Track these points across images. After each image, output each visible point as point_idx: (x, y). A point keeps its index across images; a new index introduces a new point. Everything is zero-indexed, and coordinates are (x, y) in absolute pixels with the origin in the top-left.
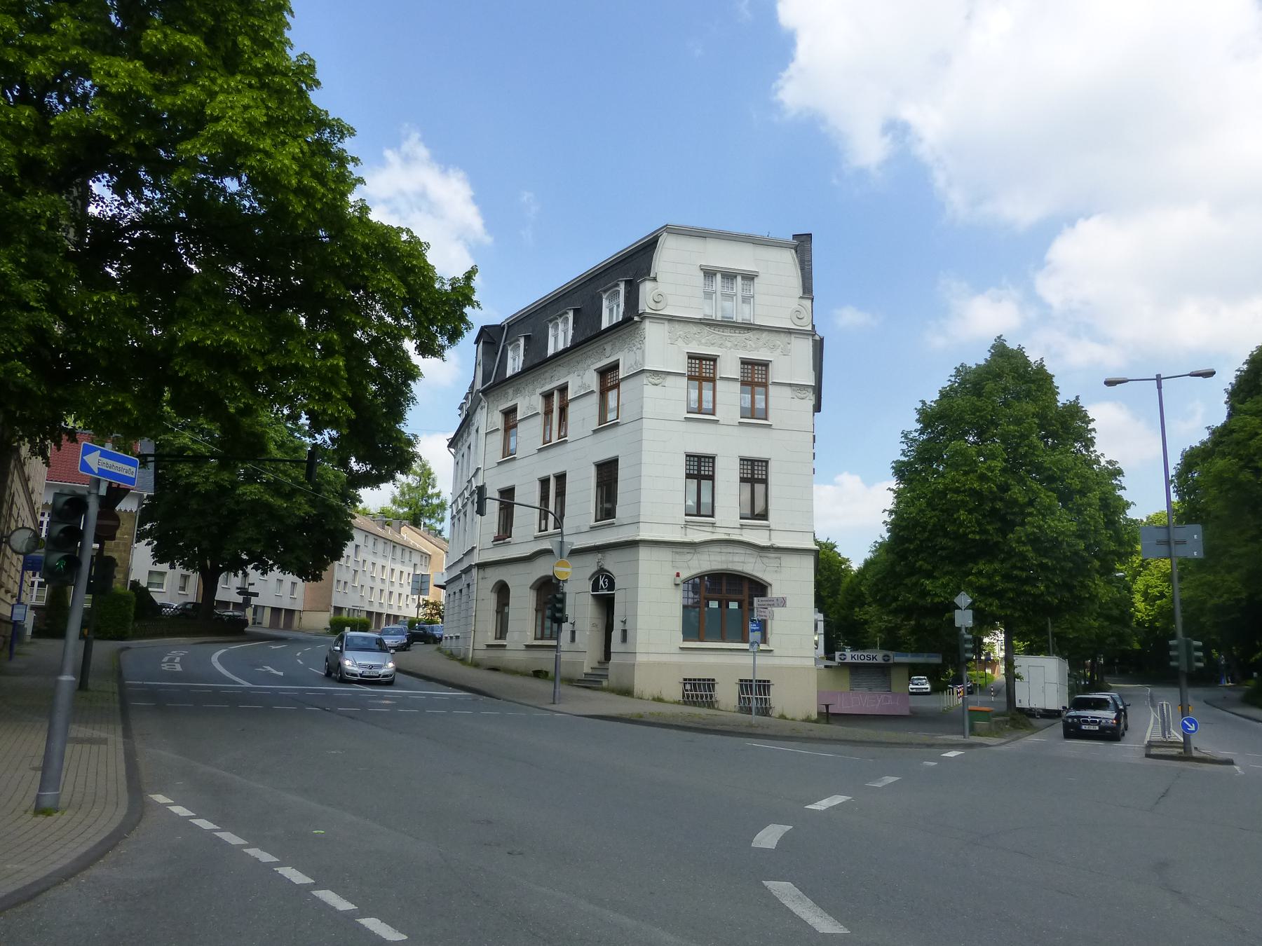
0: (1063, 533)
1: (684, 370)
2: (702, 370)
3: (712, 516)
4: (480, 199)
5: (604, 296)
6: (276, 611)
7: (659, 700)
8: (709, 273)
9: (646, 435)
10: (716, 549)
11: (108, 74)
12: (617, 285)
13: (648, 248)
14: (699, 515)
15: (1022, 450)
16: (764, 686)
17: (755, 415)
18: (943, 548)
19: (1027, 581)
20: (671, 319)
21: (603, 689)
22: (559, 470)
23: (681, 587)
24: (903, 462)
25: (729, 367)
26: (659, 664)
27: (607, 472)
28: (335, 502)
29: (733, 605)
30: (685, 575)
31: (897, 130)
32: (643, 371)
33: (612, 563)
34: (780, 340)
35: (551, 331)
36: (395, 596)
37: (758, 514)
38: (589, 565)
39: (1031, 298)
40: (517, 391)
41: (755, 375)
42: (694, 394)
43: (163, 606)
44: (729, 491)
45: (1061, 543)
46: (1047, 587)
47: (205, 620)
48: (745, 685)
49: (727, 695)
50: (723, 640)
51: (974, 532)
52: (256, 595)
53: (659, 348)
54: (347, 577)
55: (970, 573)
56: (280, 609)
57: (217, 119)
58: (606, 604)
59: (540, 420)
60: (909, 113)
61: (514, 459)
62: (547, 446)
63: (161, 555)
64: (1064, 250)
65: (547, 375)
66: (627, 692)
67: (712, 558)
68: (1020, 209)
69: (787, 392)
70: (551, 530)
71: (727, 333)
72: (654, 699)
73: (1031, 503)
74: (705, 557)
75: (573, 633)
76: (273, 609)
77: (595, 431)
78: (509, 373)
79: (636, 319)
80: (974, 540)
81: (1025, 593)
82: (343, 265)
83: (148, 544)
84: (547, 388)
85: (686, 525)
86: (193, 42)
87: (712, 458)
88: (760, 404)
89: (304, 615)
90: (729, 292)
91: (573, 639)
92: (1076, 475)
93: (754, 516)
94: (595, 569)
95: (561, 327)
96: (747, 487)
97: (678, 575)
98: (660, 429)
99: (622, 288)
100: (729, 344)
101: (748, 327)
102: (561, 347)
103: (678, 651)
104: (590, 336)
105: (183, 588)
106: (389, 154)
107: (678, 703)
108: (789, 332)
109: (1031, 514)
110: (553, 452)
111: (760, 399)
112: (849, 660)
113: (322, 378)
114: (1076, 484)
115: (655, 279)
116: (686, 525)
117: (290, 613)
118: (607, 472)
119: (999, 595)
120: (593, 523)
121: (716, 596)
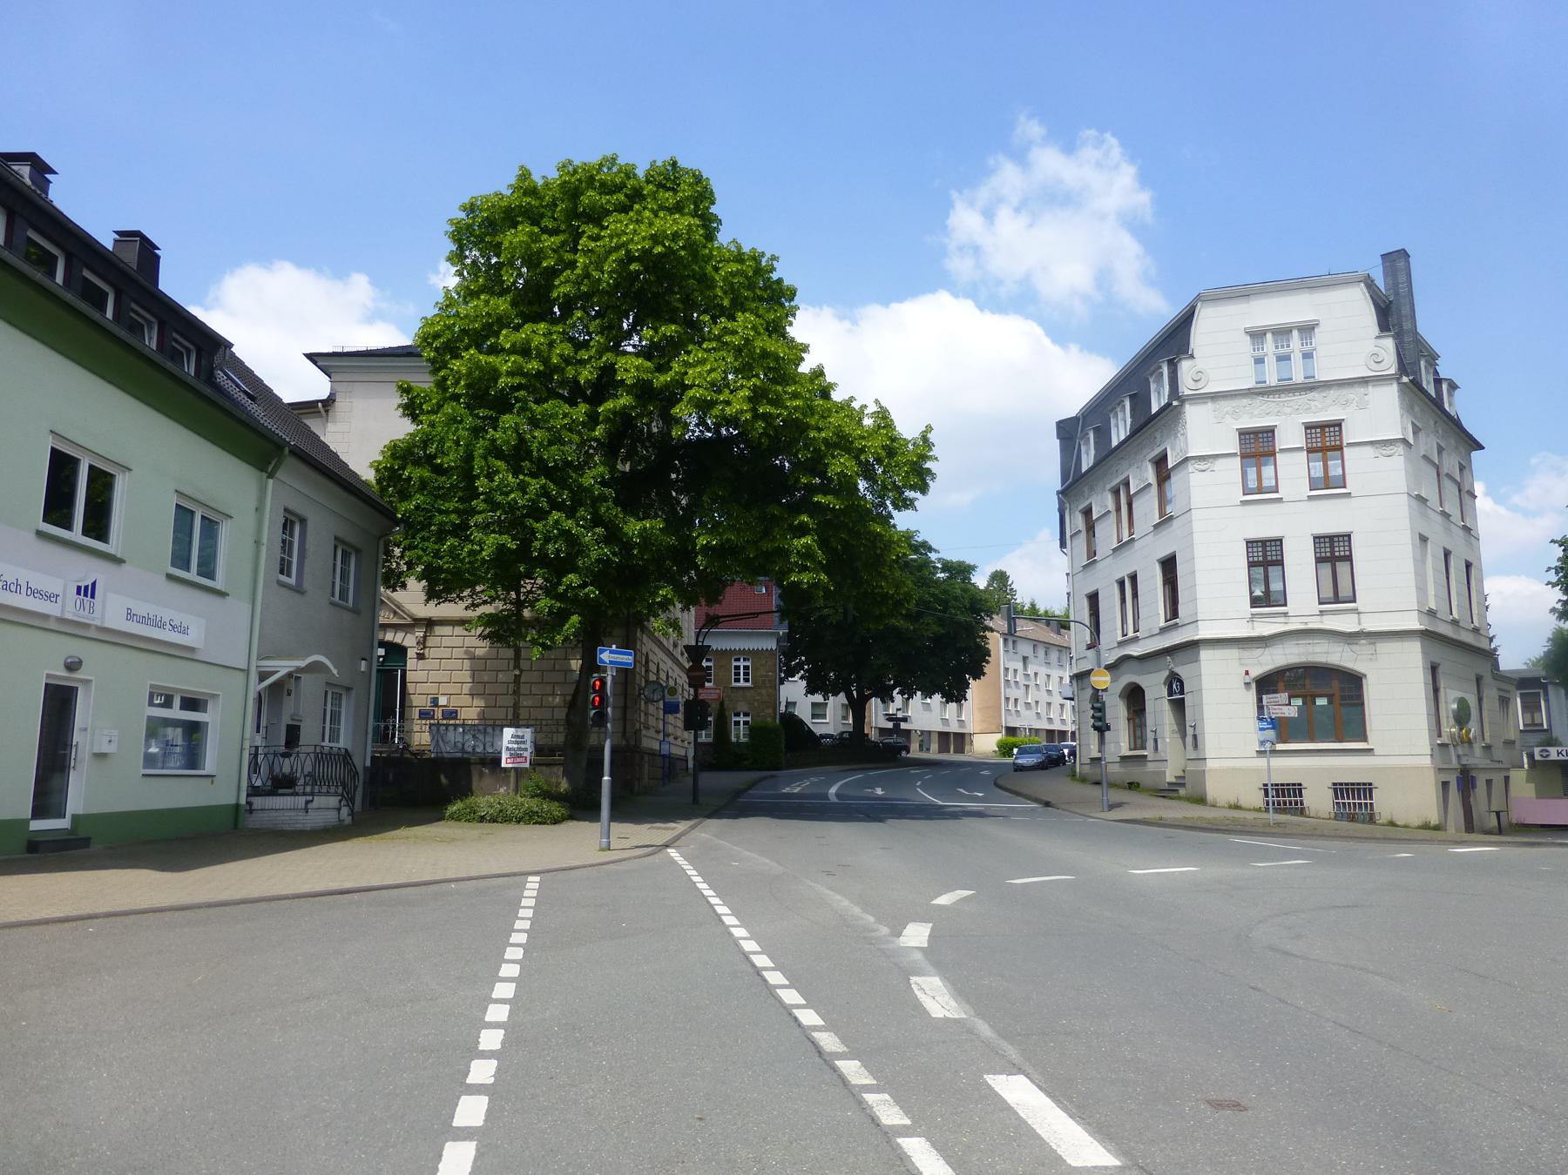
2: (1257, 446)
3: (1354, 601)
6: (944, 736)
7: (1237, 807)
8: (1257, 335)
9: (1196, 526)
17: (1328, 484)
20: (1215, 397)
21: (1180, 798)
22: (1130, 571)
25: (1290, 435)
27: (1169, 565)
30: (1256, 672)
32: (1187, 459)
34: (1353, 394)
35: (1113, 422)
37: (1338, 595)
40: (1092, 489)
41: (1325, 440)
43: (822, 736)
44: (1300, 572)
49: (1319, 800)
50: (1312, 740)
52: (905, 720)
53: (1205, 432)
57: (691, 387)
58: (1179, 706)
59: (1113, 517)
66: (1200, 800)
70: (1131, 634)
71: (1284, 398)
72: (1230, 807)
76: (940, 734)
77: (1156, 526)
86: (670, 330)
87: (1347, 537)
90: (1285, 350)
91: (1156, 749)
93: (1337, 599)
95: (1120, 415)
96: (1326, 570)
98: (1214, 519)
99: (1165, 370)
100: (1288, 410)
101: (1312, 386)
102: (1122, 437)
108: (1364, 381)
115: (1192, 357)
118: (1169, 565)
120: (1162, 624)
121: (1298, 692)
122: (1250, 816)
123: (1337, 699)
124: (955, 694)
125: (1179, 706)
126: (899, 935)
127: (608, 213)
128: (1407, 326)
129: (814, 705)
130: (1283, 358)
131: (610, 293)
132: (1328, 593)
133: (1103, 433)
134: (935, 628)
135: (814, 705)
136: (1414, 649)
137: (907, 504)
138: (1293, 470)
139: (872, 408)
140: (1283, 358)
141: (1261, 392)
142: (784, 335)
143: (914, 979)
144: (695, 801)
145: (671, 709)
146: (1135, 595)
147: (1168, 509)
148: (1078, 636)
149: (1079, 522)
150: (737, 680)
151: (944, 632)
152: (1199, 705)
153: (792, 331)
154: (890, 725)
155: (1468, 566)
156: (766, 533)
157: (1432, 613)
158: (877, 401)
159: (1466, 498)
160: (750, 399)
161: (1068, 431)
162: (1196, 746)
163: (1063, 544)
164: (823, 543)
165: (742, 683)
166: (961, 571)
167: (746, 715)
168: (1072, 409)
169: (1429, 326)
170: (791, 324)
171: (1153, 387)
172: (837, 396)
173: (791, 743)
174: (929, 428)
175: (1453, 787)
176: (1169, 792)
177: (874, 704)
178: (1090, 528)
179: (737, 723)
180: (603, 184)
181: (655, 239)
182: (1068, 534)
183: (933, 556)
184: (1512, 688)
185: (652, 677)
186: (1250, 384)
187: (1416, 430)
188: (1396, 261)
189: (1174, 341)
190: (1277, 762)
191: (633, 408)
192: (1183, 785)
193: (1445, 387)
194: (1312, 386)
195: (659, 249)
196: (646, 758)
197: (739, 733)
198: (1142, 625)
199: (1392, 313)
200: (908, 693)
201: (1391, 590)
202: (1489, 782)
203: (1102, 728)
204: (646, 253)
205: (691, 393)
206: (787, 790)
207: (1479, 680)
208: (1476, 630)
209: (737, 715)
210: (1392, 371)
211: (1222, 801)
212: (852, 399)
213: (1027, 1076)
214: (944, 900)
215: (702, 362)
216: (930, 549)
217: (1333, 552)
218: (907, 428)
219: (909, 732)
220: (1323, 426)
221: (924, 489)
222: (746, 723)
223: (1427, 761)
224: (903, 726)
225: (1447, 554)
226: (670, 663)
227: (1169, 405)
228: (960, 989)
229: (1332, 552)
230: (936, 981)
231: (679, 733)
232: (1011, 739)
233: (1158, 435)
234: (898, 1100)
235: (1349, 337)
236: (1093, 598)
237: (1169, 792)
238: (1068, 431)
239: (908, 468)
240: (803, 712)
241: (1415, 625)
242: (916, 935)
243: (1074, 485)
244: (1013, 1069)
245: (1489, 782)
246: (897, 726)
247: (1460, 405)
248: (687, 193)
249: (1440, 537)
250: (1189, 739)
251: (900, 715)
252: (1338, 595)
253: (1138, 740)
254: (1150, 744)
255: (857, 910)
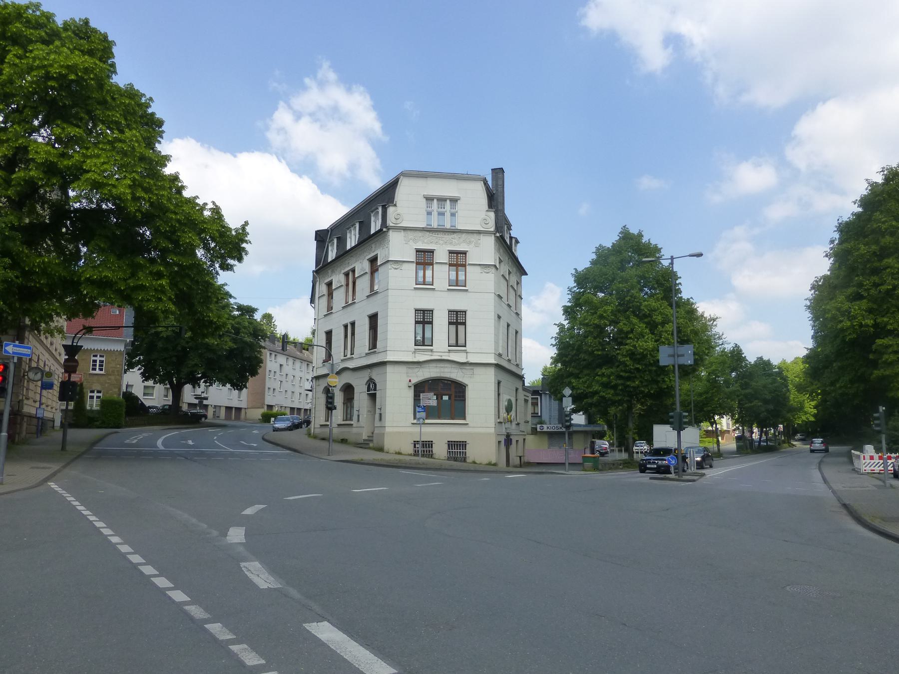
0: (646, 349)
2: (425, 258)
4: (378, 106)
6: (229, 409)
7: (399, 453)
8: (429, 199)
9: (390, 299)
10: (434, 365)
11: (36, 152)
14: (424, 345)
15: (628, 298)
19: (628, 379)
20: (405, 229)
21: (370, 448)
22: (351, 320)
25: (441, 256)
28: (248, 339)
29: (446, 398)
30: (415, 380)
31: (673, 41)
33: (375, 374)
35: (348, 235)
37: (458, 343)
38: (364, 376)
39: (782, 164)
40: (333, 272)
41: (458, 260)
42: (421, 273)
45: (646, 355)
46: (641, 382)
47: (173, 416)
48: (451, 444)
49: (440, 450)
50: (439, 418)
51: (598, 350)
52: (206, 399)
53: (398, 248)
54: (276, 385)
56: (231, 408)
57: (88, 172)
58: (373, 397)
59: (343, 290)
60: (686, 27)
63: (146, 376)
64: (805, 127)
66: (381, 449)
68: (767, 96)
69: (478, 269)
70: (349, 356)
71: (440, 235)
73: (632, 331)
77: (368, 297)
78: (330, 259)
80: (598, 355)
81: (628, 386)
82: (166, 231)
83: (139, 369)
84: (346, 270)
85: (415, 351)
86: (73, 131)
88: (461, 277)
89: (248, 411)
91: (358, 421)
92: (661, 313)
95: (353, 232)
96: (453, 328)
98: (400, 294)
99: (380, 209)
100: (441, 242)
101: (454, 231)
102: (353, 245)
104: (367, 239)
105: (166, 396)
106: (307, 81)
107: (411, 455)
108: (479, 232)
109: (631, 338)
110: (349, 309)
112: (545, 429)
113: (156, 290)
114: (659, 319)
115: (395, 205)
116: (415, 351)
117: (238, 410)
119: (614, 387)
120: (367, 351)
122: (408, 458)
124: (238, 384)
125: (373, 397)
126: (226, 535)
127: (31, 42)
128: (500, 208)
129: (145, 387)
130: (441, 214)
131: (28, 97)
132: (453, 342)
133: (342, 241)
134: (231, 344)
135: (145, 387)
136: (491, 373)
137: (226, 267)
138: (441, 274)
139: (210, 206)
140: (441, 214)
142: (153, 149)
143: (242, 564)
144: (63, 448)
145: (47, 386)
146: (353, 334)
147: (376, 288)
148: (319, 354)
149: (322, 289)
150: (94, 369)
151: (239, 348)
152: (384, 398)
153: (158, 147)
154: (196, 401)
155: (517, 332)
156: (133, 275)
157: (500, 355)
158: (214, 203)
159: (519, 299)
160: (130, 187)
161: (322, 237)
162: (380, 419)
163: (312, 301)
164: (173, 284)
165: (98, 372)
166: (248, 311)
167: (99, 392)
168: (325, 224)
169: (510, 211)
170: (160, 142)
171: (373, 219)
172: (186, 194)
173: (131, 410)
174: (246, 223)
175: (503, 443)
176: (364, 445)
177: (188, 388)
178: (330, 294)
179: (92, 397)
180: (28, 21)
181: (71, 68)
182: (317, 296)
183: (232, 301)
184: (529, 395)
185: (34, 365)
186: (423, 225)
187: (500, 261)
188: (498, 173)
189: (385, 196)
190: (425, 429)
191: (42, 179)
192: (372, 441)
193: (514, 241)
194: (454, 231)
195: (73, 77)
196: (25, 419)
197: (93, 404)
198: (356, 351)
199: (495, 199)
200: (210, 382)
201: (482, 342)
202: (517, 441)
203: (330, 407)
204: (61, 77)
205: (89, 175)
206: (127, 441)
207: (517, 389)
208: (517, 365)
209: (92, 392)
210: (492, 229)
211: (392, 450)
212: (197, 197)
213: (328, 621)
214: (249, 511)
215: (98, 156)
216: (231, 296)
217: (457, 319)
218: (233, 222)
219: (207, 406)
220: (457, 253)
221: (240, 259)
222: (98, 397)
223: (493, 430)
224: (205, 402)
225: (508, 325)
226: (47, 355)
227: (381, 230)
228: (274, 570)
229: (457, 319)
230: (257, 564)
231: (54, 404)
232: (270, 412)
233: (373, 246)
234: (254, 648)
235: (473, 210)
236: (329, 334)
237: (364, 445)
238: (322, 237)
239: (232, 246)
240: (138, 391)
241: (492, 361)
242: (236, 535)
243: (322, 267)
244: (321, 618)
245: (517, 441)
246: (201, 402)
247: (520, 252)
248: (100, 48)
249: (507, 317)
250: (377, 416)
251: (204, 395)
252: (458, 343)
253: (348, 416)
254: (355, 417)
255: (194, 520)
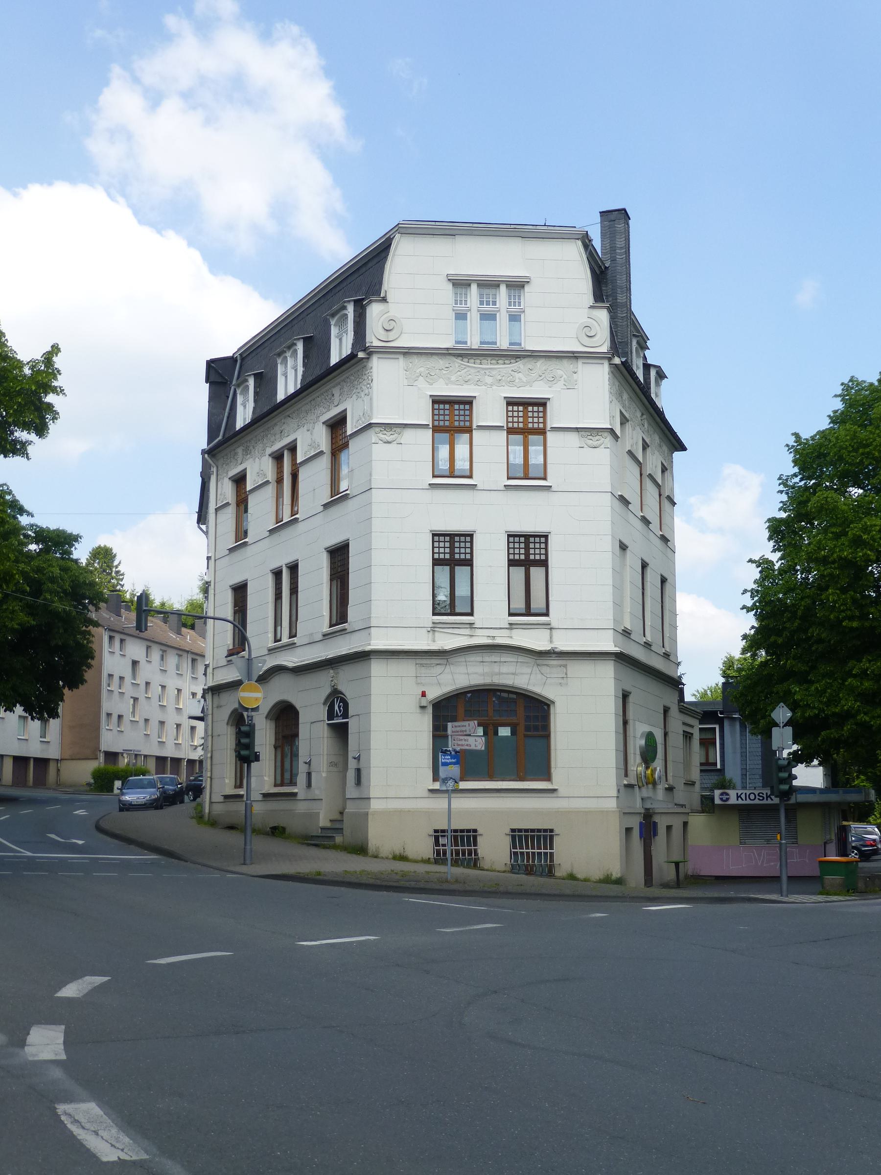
1: (427, 419)
2: (452, 417)
5: (333, 322)
7: (402, 858)
8: (460, 284)
12: (345, 308)
13: (379, 253)
14: (453, 613)
16: (544, 837)
17: (527, 476)
18: (820, 641)
20: (408, 352)
21: (335, 847)
22: (290, 559)
23: (430, 710)
24: (781, 521)
25: (490, 411)
26: (400, 812)
28: (59, 606)
29: (504, 731)
30: (434, 693)
32: (370, 426)
33: (346, 680)
34: (562, 369)
36: (170, 728)
37: (529, 608)
41: (528, 419)
49: (495, 850)
50: (491, 778)
51: (851, 618)
53: (393, 393)
55: (850, 674)
59: (270, 491)
61: (245, 544)
62: (280, 527)
65: (277, 429)
66: (361, 849)
67: (471, 670)
71: (487, 364)
74: (462, 669)
75: (309, 774)
77: (326, 506)
78: (239, 424)
79: (361, 355)
80: (852, 629)
84: (278, 446)
85: (435, 628)
89: (64, 766)
91: (309, 785)
94: (328, 691)
95: (290, 362)
96: (519, 573)
97: (424, 694)
98: (398, 499)
99: (350, 310)
100: (489, 380)
101: (516, 355)
102: (291, 390)
103: (426, 794)
104: (322, 377)
107: (427, 861)
108: (574, 356)
111: (536, 452)
112: (733, 800)
115: (384, 300)
116: (435, 628)
117: (42, 763)
120: (326, 629)
123: (521, 729)
138: (490, 452)
140: (488, 317)
141: (460, 353)
194: (516, 355)
199: (608, 280)
217: (529, 553)
252: (529, 608)
